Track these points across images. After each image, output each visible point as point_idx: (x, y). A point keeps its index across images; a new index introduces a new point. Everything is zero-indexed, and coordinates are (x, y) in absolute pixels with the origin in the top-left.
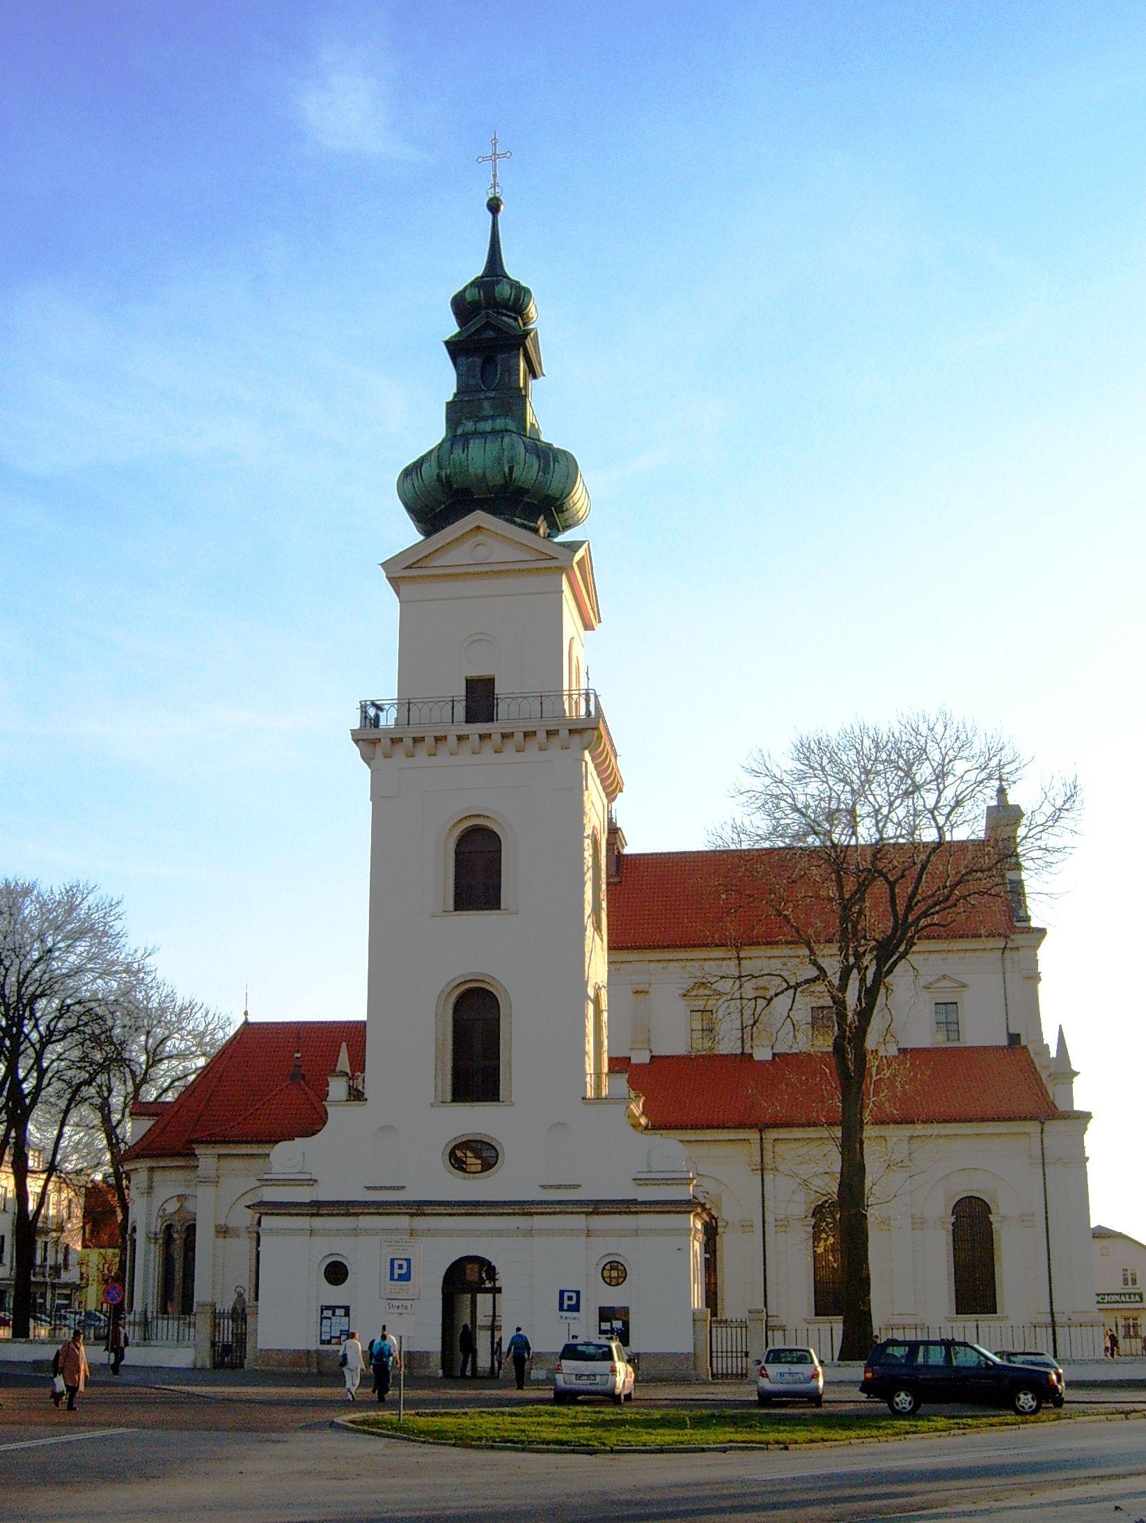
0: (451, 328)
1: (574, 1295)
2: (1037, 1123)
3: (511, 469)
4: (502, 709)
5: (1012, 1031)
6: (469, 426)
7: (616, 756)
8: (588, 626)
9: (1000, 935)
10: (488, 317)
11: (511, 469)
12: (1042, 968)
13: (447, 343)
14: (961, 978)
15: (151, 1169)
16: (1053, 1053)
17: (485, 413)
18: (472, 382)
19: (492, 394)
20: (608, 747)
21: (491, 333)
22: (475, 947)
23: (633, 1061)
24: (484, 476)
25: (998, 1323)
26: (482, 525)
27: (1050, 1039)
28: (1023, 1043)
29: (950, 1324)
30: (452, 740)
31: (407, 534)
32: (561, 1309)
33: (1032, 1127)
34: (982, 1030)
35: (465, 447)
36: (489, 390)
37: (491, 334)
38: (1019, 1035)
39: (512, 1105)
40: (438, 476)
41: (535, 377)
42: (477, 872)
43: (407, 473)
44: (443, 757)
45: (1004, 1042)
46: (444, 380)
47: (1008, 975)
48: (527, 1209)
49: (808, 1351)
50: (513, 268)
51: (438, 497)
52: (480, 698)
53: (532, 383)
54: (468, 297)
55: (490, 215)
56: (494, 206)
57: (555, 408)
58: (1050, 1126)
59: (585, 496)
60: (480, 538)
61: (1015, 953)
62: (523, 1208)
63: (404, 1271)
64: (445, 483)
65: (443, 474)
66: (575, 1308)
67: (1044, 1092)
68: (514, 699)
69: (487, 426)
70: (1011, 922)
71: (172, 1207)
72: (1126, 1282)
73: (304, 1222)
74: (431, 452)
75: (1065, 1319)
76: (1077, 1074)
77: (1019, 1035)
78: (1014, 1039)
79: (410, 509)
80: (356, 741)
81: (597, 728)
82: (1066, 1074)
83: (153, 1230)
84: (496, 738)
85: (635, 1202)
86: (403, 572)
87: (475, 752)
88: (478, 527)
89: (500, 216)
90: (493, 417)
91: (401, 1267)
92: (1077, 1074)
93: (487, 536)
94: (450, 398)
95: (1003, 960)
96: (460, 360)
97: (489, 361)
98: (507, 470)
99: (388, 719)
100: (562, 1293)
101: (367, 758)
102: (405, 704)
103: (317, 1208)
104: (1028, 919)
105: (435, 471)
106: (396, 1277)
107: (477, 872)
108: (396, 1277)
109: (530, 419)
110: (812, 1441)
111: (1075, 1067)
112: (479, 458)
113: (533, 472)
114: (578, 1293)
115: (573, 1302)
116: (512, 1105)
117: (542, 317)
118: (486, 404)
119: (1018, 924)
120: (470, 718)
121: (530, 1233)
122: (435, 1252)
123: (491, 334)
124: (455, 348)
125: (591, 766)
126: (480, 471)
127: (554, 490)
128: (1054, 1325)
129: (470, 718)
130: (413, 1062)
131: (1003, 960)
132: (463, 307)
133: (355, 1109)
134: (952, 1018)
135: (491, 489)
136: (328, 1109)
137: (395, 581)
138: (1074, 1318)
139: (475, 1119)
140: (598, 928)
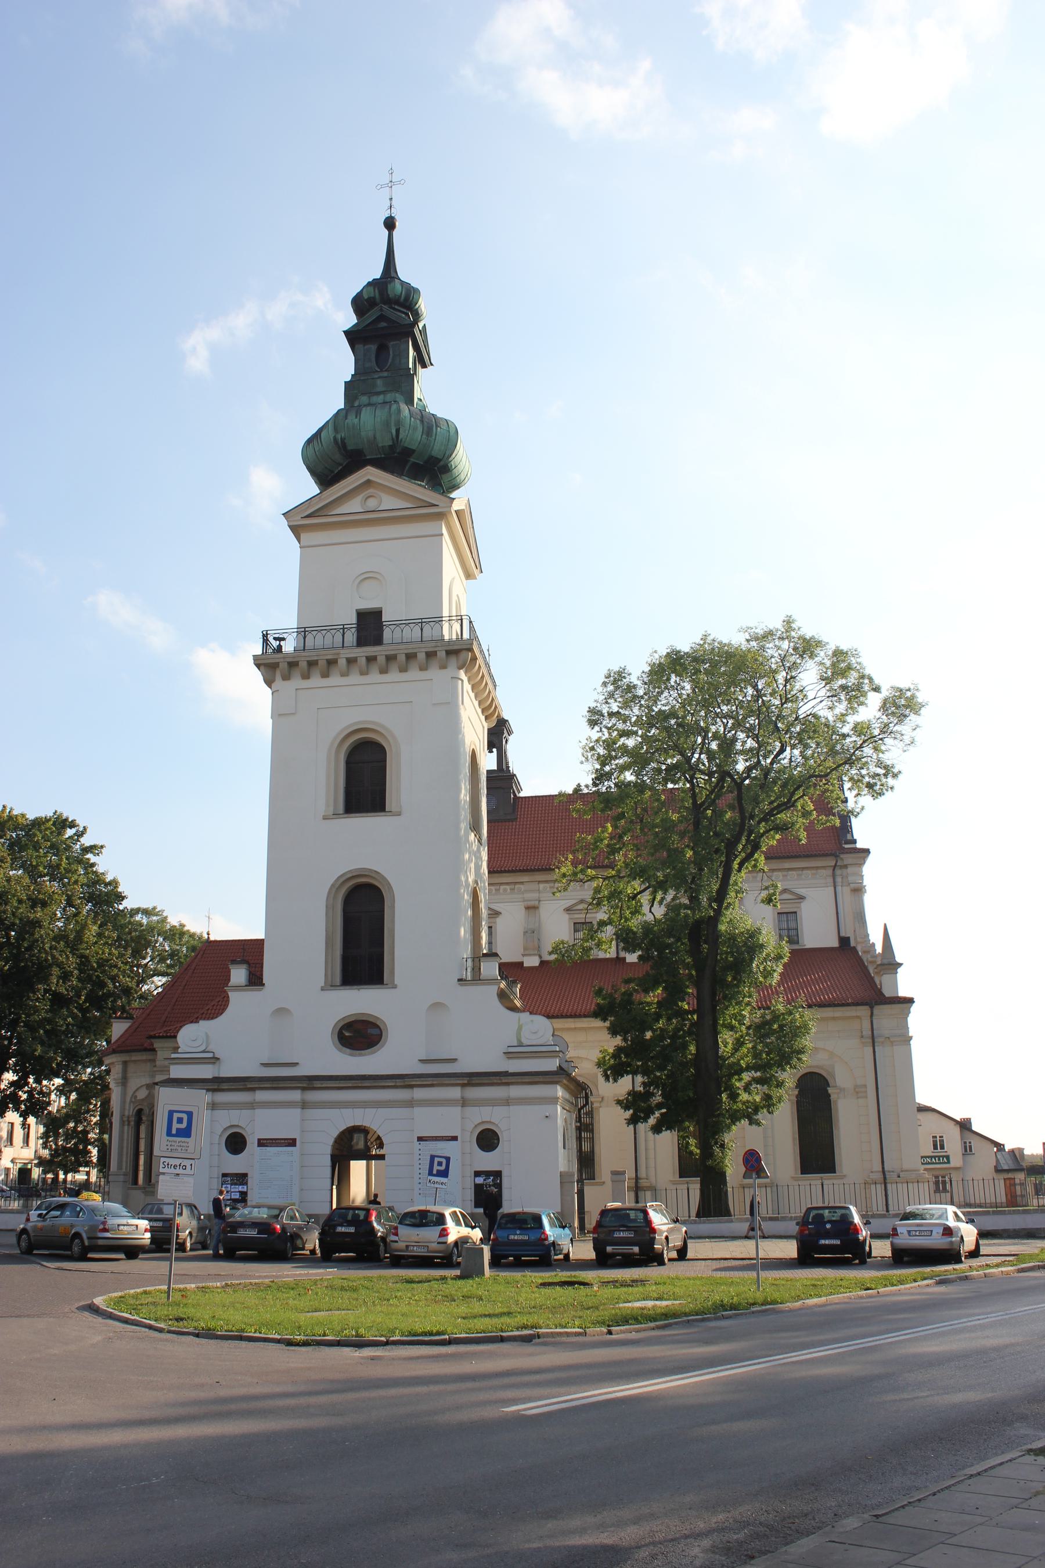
0: (349, 319)
1: (185, 1117)
2: (867, 1007)
3: (398, 431)
4: (387, 634)
5: (843, 934)
6: (364, 399)
7: (495, 686)
8: (469, 575)
9: (831, 855)
10: (381, 310)
11: (398, 431)
13: (346, 333)
14: (802, 892)
15: (125, 1063)
16: (879, 949)
17: (378, 390)
18: (368, 365)
19: (385, 374)
20: (484, 669)
21: (386, 325)
22: (365, 844)
23: (525, 965)
24: (375, 438)
25: (841, 1182)
26: (371, 478)
27: (876, 938)
28: (853, 944)
29: (796, 1183)
30: (342, 662)
31: (309, 488)
32: (431, 1173)
33: (863, 1011)
34: (818, 933)
35: (358, 414)
36: (381, 371)
37: (383, 324)
38: (848, 938)
39: (395, 987)
40: (335, 439)
41: (424, 366)
42: (365, 779)
43: (309, 441)
44: (335, 680)
45: (834, 943)
46: (343, 363)
47: (839, 888)
48: (408, 1082)
49: (848, 1208)
50: (405, 272)
51: (335, 458)
52: (370, 625)
53: (421, 371)
56: (390, 224)
58: (877, 1010)
59: (465, 458)
60: (371, 491)
61: (844, 871)
63: (184, 1125)
64: (341, 445)
65: (339, 437)
66: (444, 1174)
67: (871, 980)
68: (398, 625)
69: (380, 399)
70: (841, 844)
71: (142, 1094)
72: (935, 1147)
74: (328, 422)
76: (901, 964)
77: (848, 938)
78: (844, 941)
79: (308, 468)
80: (258, 666)
81: (471, 650)
82: (891, 966)
83: (127, 1113)
84: (381, 659)
85: (506, 1074)
86: (303, 522)
87: (362, 673)
89: (395, 233)
90: (383, 393)
91: (180, 1120)
92: (901, 964)
93: (384, 490)
94: (349, 379)
95: (834, 876)
96: (358, 347)
97: (382, 349)
98: (394, 432)
99: (288, 647)
100: (432, 1157)
101: (269, 682)
102: (303, 632)
104: (854, 842)
105: (332, 435)
106: (174, 1132)
107: (365, 779)
108: (174, 1132)
109: (417, 394)
111: (898, 960)
112: (369, 422)
113: (418, 434)
114: (448, 1159)
115: (443, 1168)
116: (395, 987)
117: (433, 316)
118: (379, 382)
119: (846, 846)
120: (361, 642)
121: (410, 1104)
122: (330, 1122)
123: (383, 324)
124: (352, 336)
125: (467, 687)
126: (371, 434)
127: (436, 452)
129: (361, 642)
130: (305, 956)
131: (834, 876)
132: (360, 304)
133: (253, 996)
134: (792, 925)
135: (382, 449)
136: (230, 994)
137: (296, 530)
139: (361, 1001)
140: (475, 827)
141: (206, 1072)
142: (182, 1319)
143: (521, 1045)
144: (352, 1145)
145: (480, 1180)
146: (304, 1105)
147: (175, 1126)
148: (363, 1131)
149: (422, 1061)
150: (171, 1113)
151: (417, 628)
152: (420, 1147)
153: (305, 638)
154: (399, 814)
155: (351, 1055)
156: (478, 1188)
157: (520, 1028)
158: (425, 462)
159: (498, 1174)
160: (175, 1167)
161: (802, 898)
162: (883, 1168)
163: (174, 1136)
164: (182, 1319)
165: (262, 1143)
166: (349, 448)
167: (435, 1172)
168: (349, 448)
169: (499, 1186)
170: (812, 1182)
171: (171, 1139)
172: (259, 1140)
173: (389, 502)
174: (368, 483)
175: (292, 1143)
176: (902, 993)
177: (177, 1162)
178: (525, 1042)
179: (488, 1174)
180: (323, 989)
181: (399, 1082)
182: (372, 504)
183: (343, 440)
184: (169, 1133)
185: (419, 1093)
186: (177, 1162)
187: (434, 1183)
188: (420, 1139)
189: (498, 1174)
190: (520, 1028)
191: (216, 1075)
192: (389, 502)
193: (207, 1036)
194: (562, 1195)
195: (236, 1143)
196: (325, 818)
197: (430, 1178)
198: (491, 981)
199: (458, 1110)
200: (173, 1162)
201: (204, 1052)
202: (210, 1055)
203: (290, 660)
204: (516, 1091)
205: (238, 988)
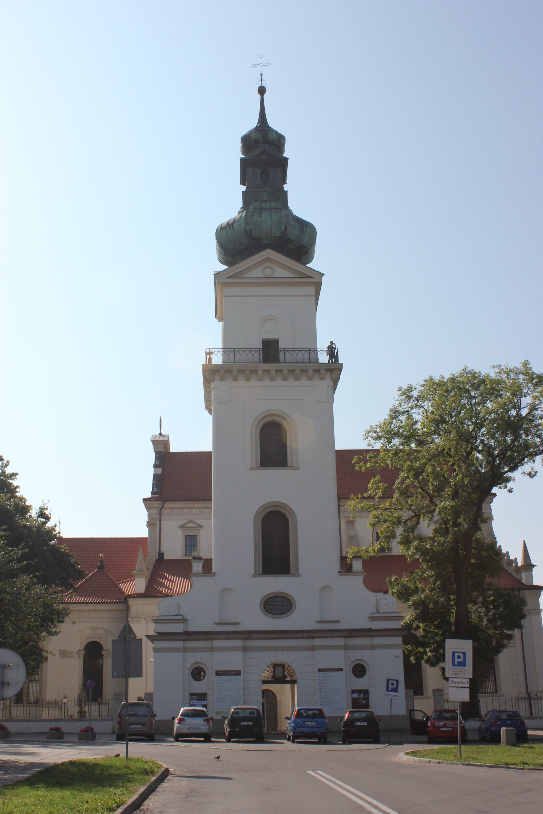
3: (286, 228)
11: (286, 228)
12: (493, 513)
14: (200, 522)
19: (268, 189)
21: (264, 158)
24: (271, 231)
26: (270, 256)
32: (387, 690)
35: (260, 215)
37: (265, 157)
39: (299, 575)
40: (245, 229)
50: (273, 123)
51: (237, 245)
52: (270, 350)
54: (253, 136)
55: (259, 96)
56: (262, 91)
57: (301, 199)
60: (268, 264)
62: (308, 634)
64: (248, 233)
65: (248, 228)
66: (395, 690)
73: (179, 644)
75: (534, 696)
76: (534, 566)
88: (268, 258)
89: (265, 96)
92: (534, 566)
93: (270, 263)
98: (283, 228)
100: (388, 680)
102: (225, 351)
103: (187, 636)
108: (456, 663)
110: (507, 766)
111: (533, 562)
112: (268, 221)
121: (313, 648)
123: (265, 157)
128: (530, 699)
132: (248, 142)
135: (266, 240)
138: (539, 695)
141: (178, 628)
142: (527, 764)
143: (378, 612)
144: (281, 675)
145: (355, 695)
146: (245, 649)
147: (457, 660)
148: (282, 666)
149: (217, 624)
150: (453, 653)
151: (306, 355)
152: (320, 675)
153: (235, 355)
154: (298, 468)
155: (273, 618)
156: (354, 700)
157: (378, 602)
158: (296, 242)
159: (366, 692)
160: (458, 683)
161: (201, 527)
162: (527, 690)
163: (456, 666)
164: (527, 764)
165: (341, 670)
166: (253, 236)
167: (390, 689)
168: (253, 236)
169: (367, 699)
170: (494, 698)
171: (454, 667)
172: (217, 672)
173: (280, 273)
174: (268, 259)
175: (238, 673)
176: (536, 583)
177: (459, 680)
178: (381, 610)
179: (360, 691)
180: (253, 576)
181: (305, 635)
182: (268, 272)
183: (250, 231)
184: (453, 664)
185: (318, 642)
186: (459, 680)
187: (390, 695)
188: (320, 670)
189: (366, 692)
190: (378, 602)
191: (185, 630)
192: (280, 273)
193: (178, 605)
194: (407, 704)
195: (198, 673)
196: (251, 469)
197: (387, 692)
198: (358, 573)
199: (342, 652)
200: (457, 680)
201: (177, 615)
202: (181, 617)
203: (226, 368)
204: (377, 641)
205: (197, 575)
